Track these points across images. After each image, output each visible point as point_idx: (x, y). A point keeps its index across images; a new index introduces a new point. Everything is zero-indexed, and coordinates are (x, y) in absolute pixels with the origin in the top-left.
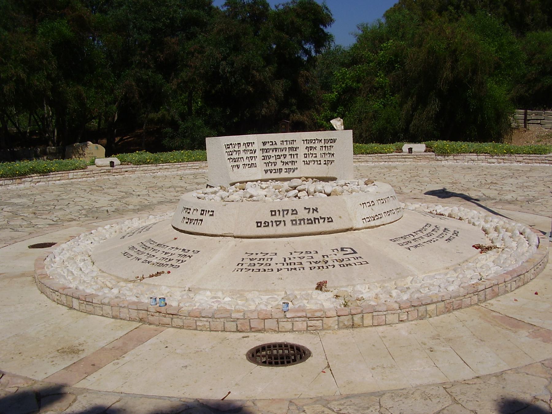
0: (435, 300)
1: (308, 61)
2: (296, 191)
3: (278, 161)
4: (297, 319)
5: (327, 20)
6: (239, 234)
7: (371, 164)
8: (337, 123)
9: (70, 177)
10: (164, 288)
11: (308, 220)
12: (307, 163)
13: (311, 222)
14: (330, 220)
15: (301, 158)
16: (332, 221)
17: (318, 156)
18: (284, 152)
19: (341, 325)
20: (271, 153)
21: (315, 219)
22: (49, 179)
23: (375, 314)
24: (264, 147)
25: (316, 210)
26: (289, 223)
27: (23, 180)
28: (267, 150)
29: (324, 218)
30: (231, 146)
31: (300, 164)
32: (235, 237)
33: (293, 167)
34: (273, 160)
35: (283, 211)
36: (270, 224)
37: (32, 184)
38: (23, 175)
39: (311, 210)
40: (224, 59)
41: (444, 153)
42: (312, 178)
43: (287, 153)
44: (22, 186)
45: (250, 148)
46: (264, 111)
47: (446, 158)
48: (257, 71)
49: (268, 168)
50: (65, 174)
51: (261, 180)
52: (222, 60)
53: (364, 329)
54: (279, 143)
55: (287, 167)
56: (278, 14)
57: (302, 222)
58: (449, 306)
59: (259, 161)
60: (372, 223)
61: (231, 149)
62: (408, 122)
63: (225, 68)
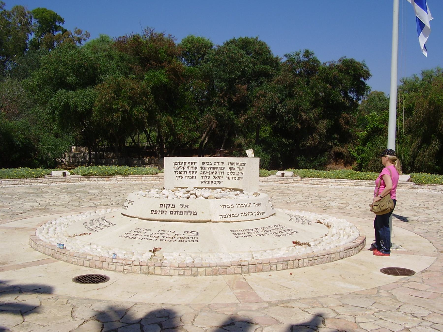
0: (204, 265)
1: (351, 106)
2: (189, 194)
3: (211, 176)
4: (118, 264)
5: (367, 75)
6: (144, 217)
7: (363, 188)
8: (250, 152)
9: (143, 180)
10: (78, 241)
11: (180, 212)
12: (229, 179)
13: (182, 213)
14: (195, 214)
15: (226, 175)
16: (196, 214)
17: (235, 174)
18: (216, 170)
19: (142, 271)
20: (207, 170)
21: (185, 211)
22: (128, 180)
23: (162, 267)
24: (203, 166)
25: (187, 206)
26: (168, 213)
27: (110, 178)
28: (204, 168)
29: (191, 212)
30: (178, 164)
31: (224, 179)
32: (140, 219)
33: (220, 180)
34: (208, 175)
35: (167, 205)
36: (158, 212)
37: (116, 182)
38: (111, 175)
39: (184, 206)
40: (281, 102)
41: (420, 183)
42: (230, 189)
43: (217, 171)
44: (108, 182)
45: (193, 165)
46: (309, 143)
47: (422, 187)
48: (304, 112)
49: (204, 180)
50: (139, 177)
51: (198, 188)
52: (279, 103)
53: (153, 276)
54: (213, 164)
55: (216, 180)
56: (325, 70)
57: (177, 213)
58: (215, 271)
59: (198, 175)
60: (228, 219)
61: (178, 165)
62: (414, 157)
63: (280, 109)
